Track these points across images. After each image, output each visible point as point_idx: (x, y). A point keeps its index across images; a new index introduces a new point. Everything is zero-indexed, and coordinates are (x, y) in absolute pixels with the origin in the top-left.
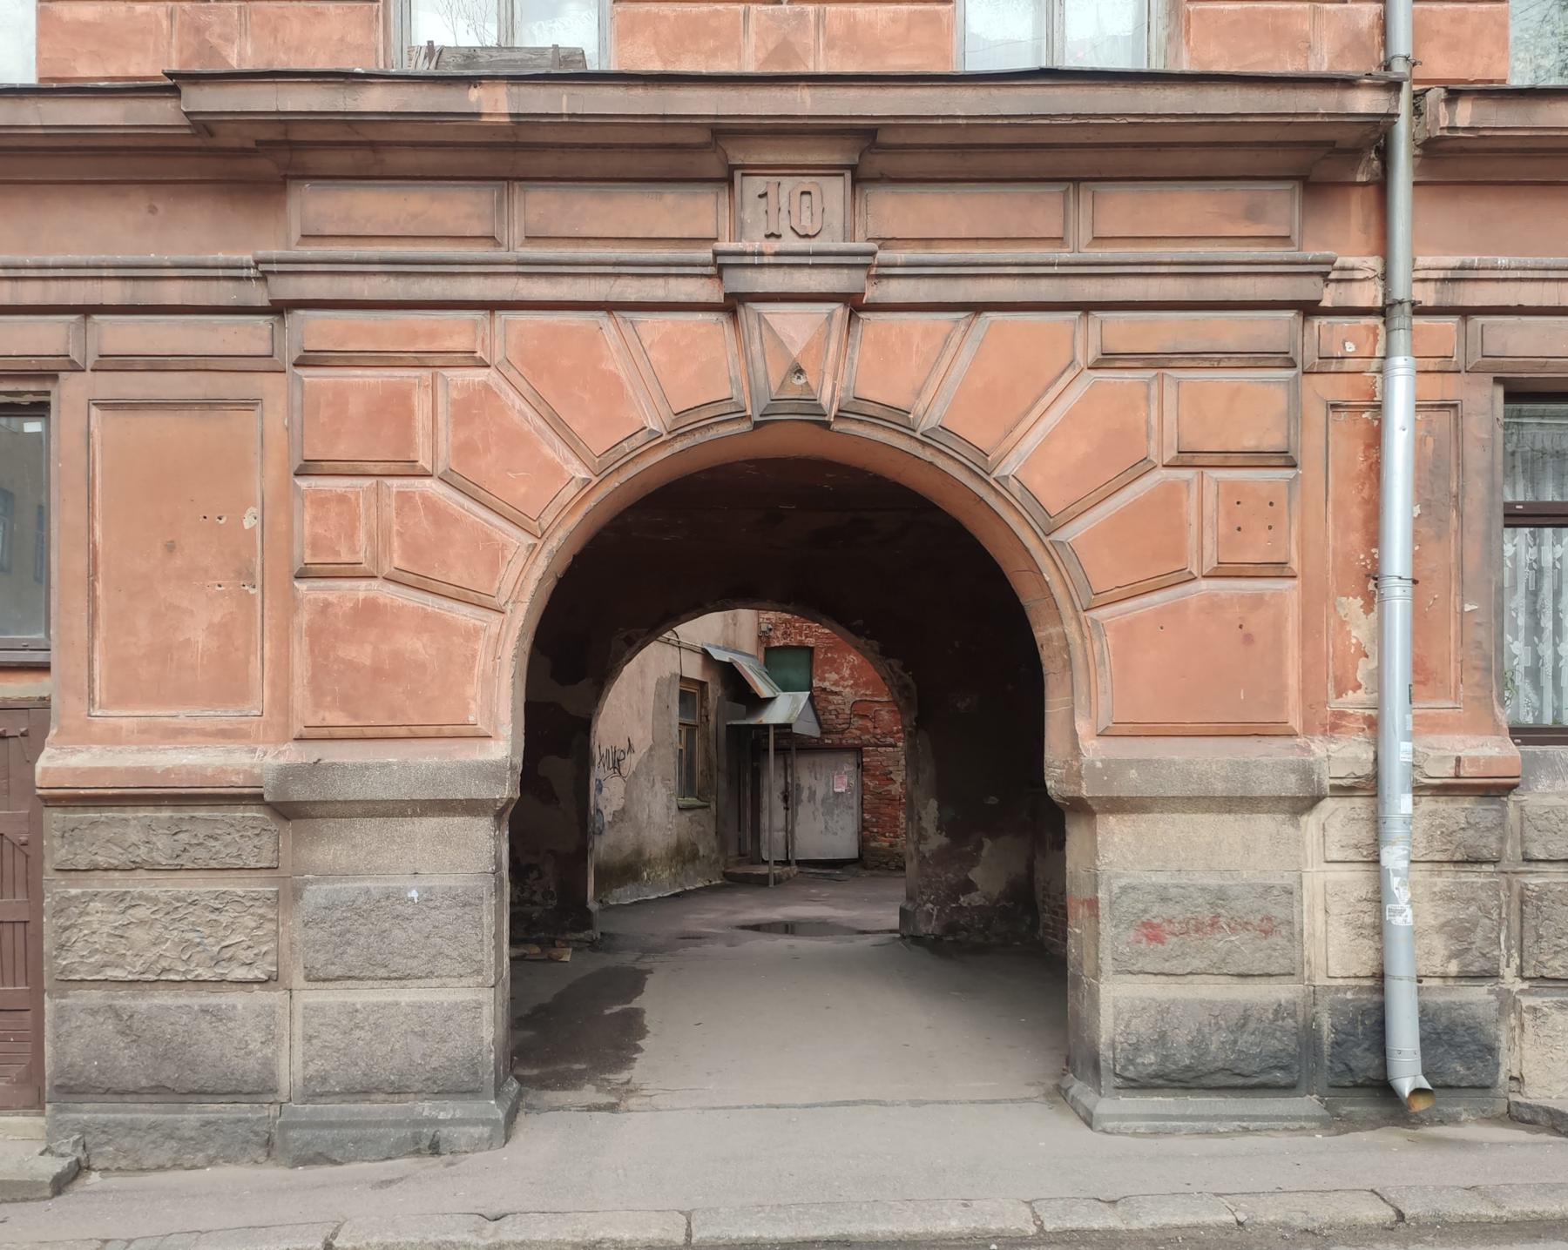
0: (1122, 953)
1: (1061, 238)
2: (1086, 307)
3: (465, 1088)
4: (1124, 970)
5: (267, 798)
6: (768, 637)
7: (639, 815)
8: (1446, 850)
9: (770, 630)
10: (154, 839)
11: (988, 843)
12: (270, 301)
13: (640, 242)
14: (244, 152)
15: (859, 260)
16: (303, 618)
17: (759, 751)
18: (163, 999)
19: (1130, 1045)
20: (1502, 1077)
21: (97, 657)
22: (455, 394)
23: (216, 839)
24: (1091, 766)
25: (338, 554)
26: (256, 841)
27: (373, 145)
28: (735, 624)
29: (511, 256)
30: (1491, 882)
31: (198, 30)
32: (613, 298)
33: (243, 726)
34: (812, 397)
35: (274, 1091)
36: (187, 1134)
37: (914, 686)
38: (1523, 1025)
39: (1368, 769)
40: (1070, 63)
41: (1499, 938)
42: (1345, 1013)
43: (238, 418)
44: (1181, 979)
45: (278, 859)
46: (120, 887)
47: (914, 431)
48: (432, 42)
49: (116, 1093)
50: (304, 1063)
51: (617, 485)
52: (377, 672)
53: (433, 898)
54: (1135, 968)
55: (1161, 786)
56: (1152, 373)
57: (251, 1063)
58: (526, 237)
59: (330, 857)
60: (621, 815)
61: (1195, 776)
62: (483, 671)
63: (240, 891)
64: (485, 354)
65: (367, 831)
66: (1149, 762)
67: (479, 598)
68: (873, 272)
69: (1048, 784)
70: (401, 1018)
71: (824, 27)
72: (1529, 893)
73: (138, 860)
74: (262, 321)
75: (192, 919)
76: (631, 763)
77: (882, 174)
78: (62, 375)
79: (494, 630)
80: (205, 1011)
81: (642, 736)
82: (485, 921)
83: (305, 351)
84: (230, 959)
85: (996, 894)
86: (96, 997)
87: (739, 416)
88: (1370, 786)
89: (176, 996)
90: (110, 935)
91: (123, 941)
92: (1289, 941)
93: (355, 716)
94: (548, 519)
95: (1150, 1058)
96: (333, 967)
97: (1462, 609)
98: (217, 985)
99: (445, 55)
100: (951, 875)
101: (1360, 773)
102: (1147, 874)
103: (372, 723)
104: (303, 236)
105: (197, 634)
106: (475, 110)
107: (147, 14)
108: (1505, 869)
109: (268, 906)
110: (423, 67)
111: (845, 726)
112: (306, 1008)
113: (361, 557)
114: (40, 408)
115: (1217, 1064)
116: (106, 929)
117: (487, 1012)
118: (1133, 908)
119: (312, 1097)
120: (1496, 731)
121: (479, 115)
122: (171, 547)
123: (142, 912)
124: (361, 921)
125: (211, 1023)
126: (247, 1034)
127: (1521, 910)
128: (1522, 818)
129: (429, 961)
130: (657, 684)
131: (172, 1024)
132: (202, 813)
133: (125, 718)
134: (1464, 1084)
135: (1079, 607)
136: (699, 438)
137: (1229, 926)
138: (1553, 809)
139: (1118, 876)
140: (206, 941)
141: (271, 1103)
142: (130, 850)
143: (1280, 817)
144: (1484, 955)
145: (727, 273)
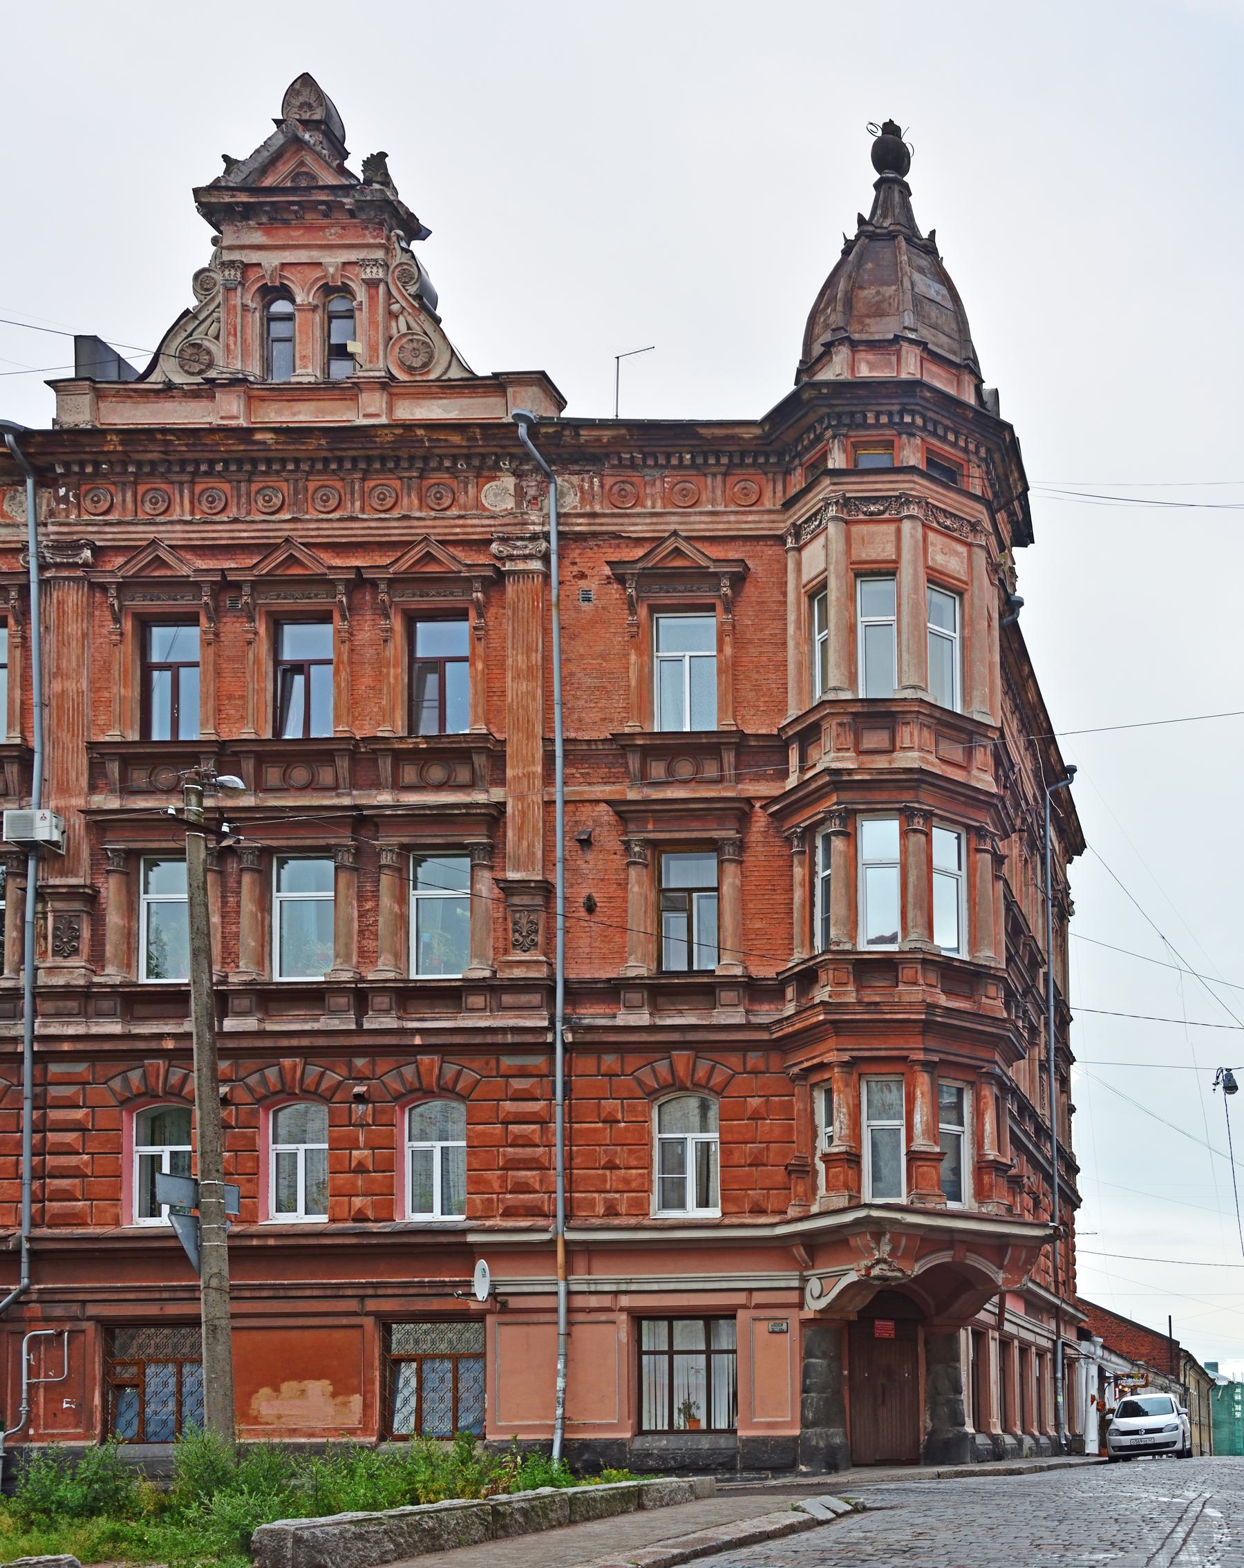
1: (858, 575)
12: (996, 393)
74: (609, 1297)
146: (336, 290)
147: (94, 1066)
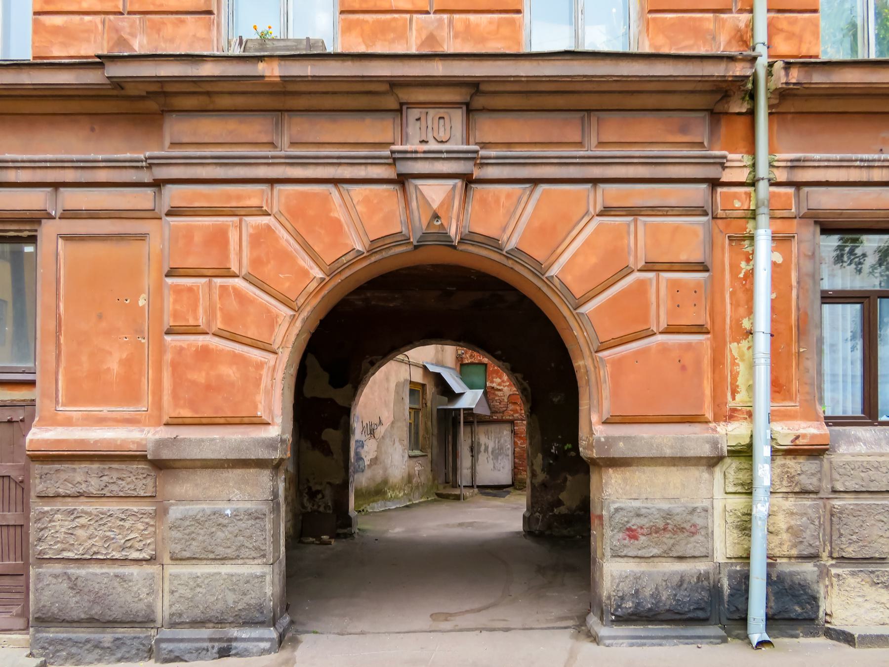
0: (615, 546)
1: (581, 143)
2: (595, 181)
3: (257, 620)
4: (616, 556)
5: (149, 457)
6: (462, 358)
7: (386, 460)
8: (791, 486)
9: (463, 353)
10: (90, 480)
11: (569, 478)
12: (154, 180)
13: (716, 60)
14: (141, 98)
15: (470, 155)
16: (168, 357)
17: (456, 423)
18: (96, 569)
19: (619, 597)
20: (821, 614)
21: (60, 377)
22: (251, 231)
23: (123, 480)
24: (599, 440)
25: (188, 320)
26: (144, 481)
27: (208, 94)
28: (443, 351)
29: (282, 153)
30: (814, 504)
31: (117, 31)
32: (337, 177)
33: (138, 417)
34: (445, 232)
35: (153, 621)
36: (106, 645)
37: (529, 390)
38: (832, 584)
39: (747, 441)
40: (588, 47)
41: (819, 534)
42: (735, 578)
43: (135, 245)
44: (647, 560)
45: (156, 492)
46: (71, 506)
47: (502, 250)
48: (242, 37)
49: (68, 622)
50: (170, 605)
51: (340, 281)
52: (208, 387)
53: (239, 514)
54: (623, 554)
55: (636, 451)
56: (630, 219)
57: (141, 606)
58: (291, 143)
59: (183, 491)
60: (375, 461)
61: (655, 445)
62: (266, 386)
63: (135, 509)
64: (268, 208)
65: (203, 478)
66: (630, 438)
67: (264, 345)
68: (478, 161)
69: (581, 449)
70: (222, 582)
71: (453, 26)
72: (835, 510)
73: (81, 491)
74: (149, 191)
75: (109, 524)
76: (380, 431)
77: (483, 107)
78: (43, 221)
79: (272, 363)
80: (117, 576)
81: (387, 416)
82: (267, 527)
83: (172, 207)
84: (130, 547)
85: (574, 507)
86: (58, 568)
87: (406, 241)
88: (745, 453)
89: (101, 568)
90: (65, 533)
91: (73, 537)
92: (705, 538)
93: (196, 412)
94: (301, 301)
95: (629, 604)
96: (185, 552)
97: (799, 351)
98: (123, 562)
99: (249, 45)
100: (549, 497)
101: (743, 443)
102: (630, 501)
103: (206, 415)
104: (171, 143)
105: (113, 365)
106: (261, 75)
107: (91, 21)
108: (822, 496)
109: (150, 518)
110: (237, 51)
111: (505, 409)
112: (170, 575)
113: (200, 322)
114: (32, 239)
115: (665, 608)
116: (63, 530)
117: (268, 578)
118: (622, 520)
119: (173, 625)
120: (817, 419)
121: (263, 77)
122: (100, 317)
123: (83, 521)
124: (200, 526)
125: (120, 583)
126: (139, 589)
127: (831, 519)
128: (831, 467)
129: (237, 550)
130: (396, 385)
131: (98, 583)
132: (115, 466)
133: (75, 411)
134: (800, 618)
135: (592, 350)
136: (384, 254)
137: (673, 530)
138: (848, 463)
139: (614, 502)
140: (117, 537)
141: (152, 628)
142: (77, 485)
143: (701, 468)
144: (811, 545)
145: (398, 164)
146: (828, 615)
147: (276, 466)
